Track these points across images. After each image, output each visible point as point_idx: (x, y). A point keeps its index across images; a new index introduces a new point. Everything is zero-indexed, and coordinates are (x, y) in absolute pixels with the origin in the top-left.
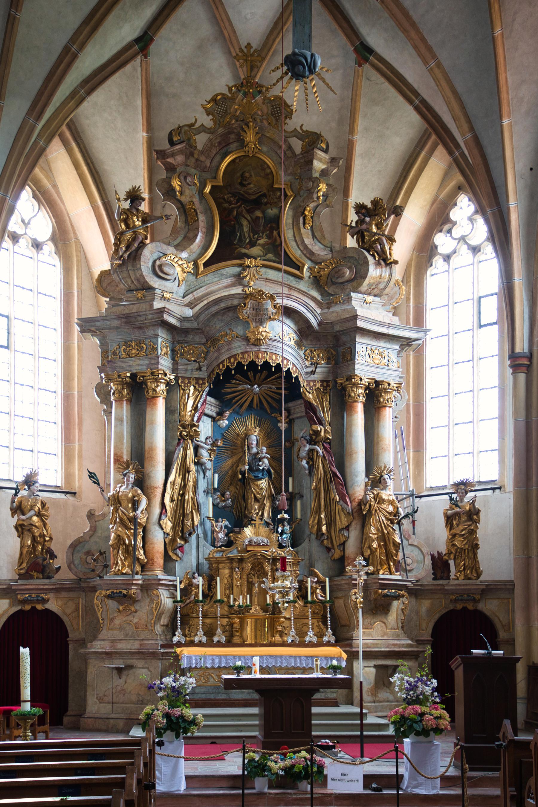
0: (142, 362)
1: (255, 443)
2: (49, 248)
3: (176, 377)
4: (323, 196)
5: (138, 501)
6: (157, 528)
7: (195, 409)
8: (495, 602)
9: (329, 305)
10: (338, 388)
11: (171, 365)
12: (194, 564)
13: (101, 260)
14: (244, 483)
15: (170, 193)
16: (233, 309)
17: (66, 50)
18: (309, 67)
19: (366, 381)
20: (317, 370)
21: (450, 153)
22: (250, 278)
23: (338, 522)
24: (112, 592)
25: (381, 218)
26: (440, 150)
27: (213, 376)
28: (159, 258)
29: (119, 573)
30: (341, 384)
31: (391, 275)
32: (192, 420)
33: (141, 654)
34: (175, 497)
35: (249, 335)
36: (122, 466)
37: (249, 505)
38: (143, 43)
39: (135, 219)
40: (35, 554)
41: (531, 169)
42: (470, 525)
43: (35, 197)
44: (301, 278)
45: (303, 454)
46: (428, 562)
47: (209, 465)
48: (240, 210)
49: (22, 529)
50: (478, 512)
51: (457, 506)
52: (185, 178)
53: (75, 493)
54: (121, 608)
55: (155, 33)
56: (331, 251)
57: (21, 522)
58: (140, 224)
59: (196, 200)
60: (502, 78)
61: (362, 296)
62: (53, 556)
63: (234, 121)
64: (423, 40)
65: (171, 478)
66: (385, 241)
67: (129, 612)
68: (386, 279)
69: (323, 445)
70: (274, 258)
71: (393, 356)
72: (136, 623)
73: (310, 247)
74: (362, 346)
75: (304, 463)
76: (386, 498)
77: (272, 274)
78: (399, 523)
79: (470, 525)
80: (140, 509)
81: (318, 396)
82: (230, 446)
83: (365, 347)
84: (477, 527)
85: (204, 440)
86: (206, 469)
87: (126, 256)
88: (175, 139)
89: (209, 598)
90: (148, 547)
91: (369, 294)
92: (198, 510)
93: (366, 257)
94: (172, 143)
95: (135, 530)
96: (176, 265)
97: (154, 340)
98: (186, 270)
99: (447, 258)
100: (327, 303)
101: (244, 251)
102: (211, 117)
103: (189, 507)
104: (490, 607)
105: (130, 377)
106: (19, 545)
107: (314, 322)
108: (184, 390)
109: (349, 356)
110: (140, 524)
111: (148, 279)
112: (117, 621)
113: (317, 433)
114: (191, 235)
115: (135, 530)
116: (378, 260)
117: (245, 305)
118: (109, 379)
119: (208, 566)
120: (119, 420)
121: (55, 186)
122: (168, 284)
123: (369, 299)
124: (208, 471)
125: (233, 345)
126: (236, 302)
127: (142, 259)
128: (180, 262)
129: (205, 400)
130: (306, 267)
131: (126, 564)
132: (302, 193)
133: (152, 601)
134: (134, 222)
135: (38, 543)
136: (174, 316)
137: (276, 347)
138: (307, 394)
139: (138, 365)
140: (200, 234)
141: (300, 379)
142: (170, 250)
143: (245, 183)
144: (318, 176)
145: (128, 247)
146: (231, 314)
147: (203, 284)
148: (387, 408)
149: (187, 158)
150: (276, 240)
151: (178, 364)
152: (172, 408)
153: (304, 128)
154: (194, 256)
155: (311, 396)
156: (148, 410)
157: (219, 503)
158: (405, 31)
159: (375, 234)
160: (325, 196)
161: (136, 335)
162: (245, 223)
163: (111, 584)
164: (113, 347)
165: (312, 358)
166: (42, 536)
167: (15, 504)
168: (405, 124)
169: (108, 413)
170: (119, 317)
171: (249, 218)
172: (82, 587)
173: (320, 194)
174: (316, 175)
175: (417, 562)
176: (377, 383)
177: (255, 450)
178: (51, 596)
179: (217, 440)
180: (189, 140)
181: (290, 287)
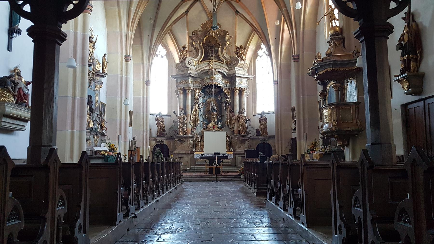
2: (165, 57)
9: (230, 70)
10: (232, 89)
13: (177, 60)
15: (192, 45)
16: (207, 72)
17: (169, 16)
19: (238, 88)
21: (258, 34)
26: (256, 34)
33: (185, 154)
36: (181, 110)
38: (187, 12)
45: (224, 106)
46: (255, 131)
47: (202, 109)
49: (158, 124)
50: (267, 119)
59: (199, 47)
60: (267, 20)
62: (165, 131)
64: (249, 11)
71: (245, 82)
74: (238, 80)
77: (216, 63)
82: (207, 104)
99: (261, 57)
100: (229, 69)
103: (197, 119)
104: (270, 142)
107: (226, 75)
109: (234, 82)
113: (227, 101)
120: (180, 98)
121: (167, 43)
123: (239, 68)
158: (244, 9)
161: (184, 79)
168: (248, 28)
170: (180, 75)
172: (171, 138)
174: (226, 40)
176: (241, 88)
181: (221, 66)
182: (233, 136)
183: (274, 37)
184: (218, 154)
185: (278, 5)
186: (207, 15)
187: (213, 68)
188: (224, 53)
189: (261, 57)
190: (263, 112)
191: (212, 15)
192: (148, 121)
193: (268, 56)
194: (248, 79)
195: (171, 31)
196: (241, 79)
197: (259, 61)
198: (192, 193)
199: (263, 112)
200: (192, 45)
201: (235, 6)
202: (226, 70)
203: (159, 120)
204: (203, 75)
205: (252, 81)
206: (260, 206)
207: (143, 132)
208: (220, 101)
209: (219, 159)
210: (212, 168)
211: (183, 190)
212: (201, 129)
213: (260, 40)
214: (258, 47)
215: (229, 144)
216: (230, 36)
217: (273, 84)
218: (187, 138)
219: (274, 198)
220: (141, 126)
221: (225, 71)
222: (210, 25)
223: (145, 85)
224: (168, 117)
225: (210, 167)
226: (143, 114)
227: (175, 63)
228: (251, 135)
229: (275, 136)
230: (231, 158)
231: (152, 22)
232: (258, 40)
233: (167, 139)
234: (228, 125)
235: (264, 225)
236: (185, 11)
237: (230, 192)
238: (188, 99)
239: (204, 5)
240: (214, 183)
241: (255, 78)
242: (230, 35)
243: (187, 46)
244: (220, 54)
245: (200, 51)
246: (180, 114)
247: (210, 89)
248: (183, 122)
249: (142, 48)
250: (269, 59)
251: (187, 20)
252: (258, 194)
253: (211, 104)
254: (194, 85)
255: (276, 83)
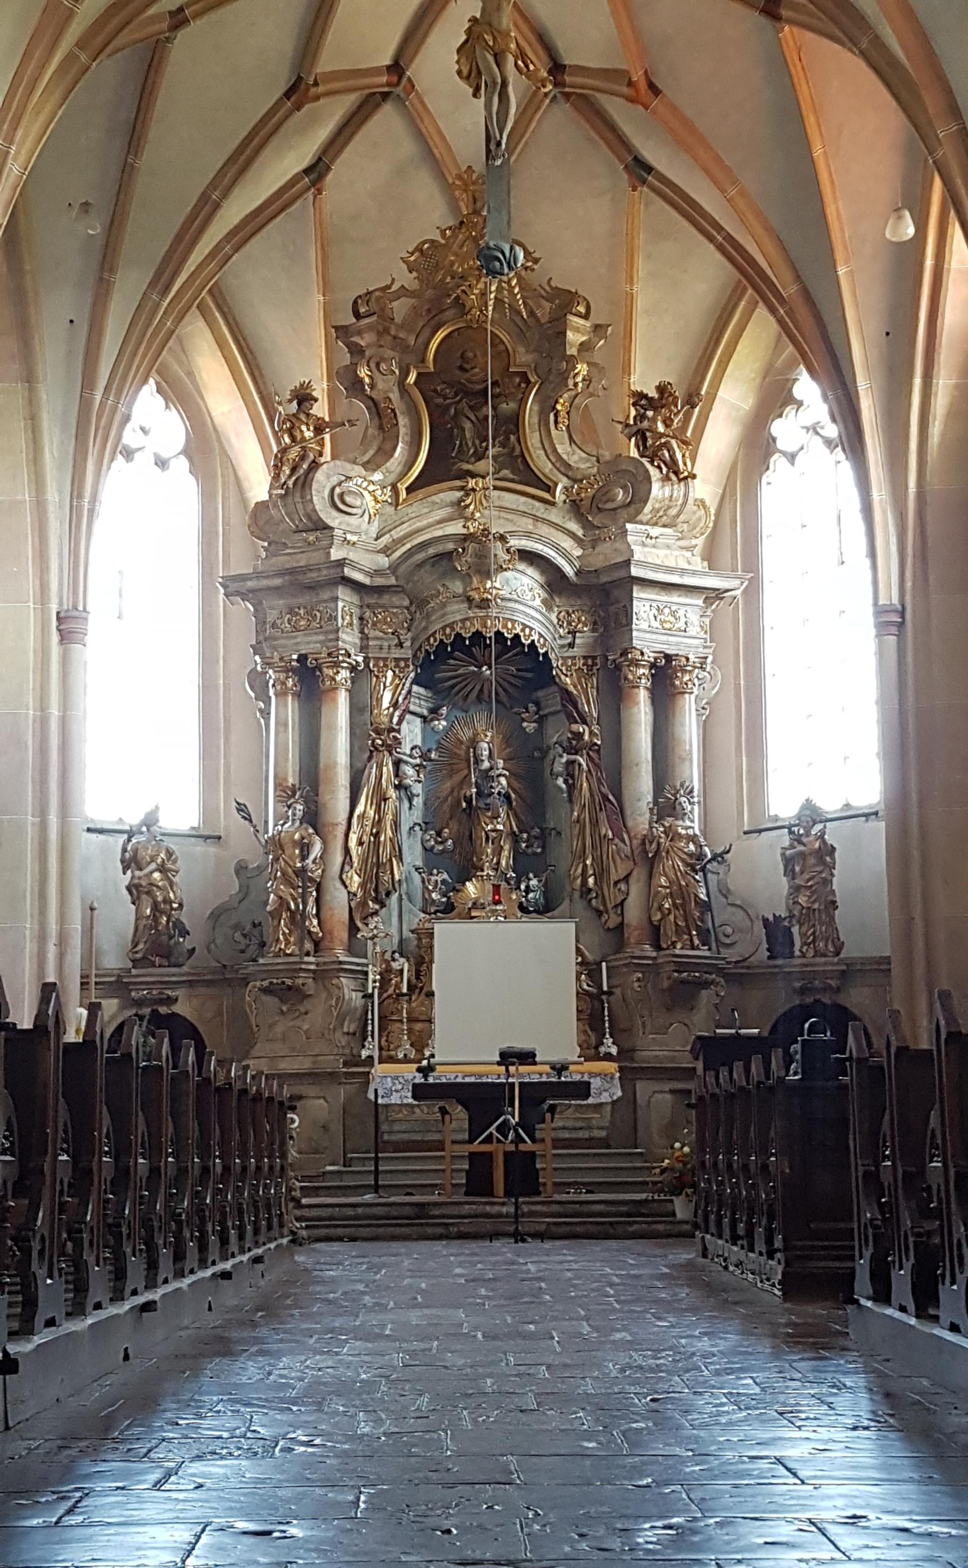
0: (315, 638)
1: (486, 753)
2: (183, 463)
3: (365, 658)
4: (584, 380)
5: (308, 845)
6: (338, 884)
7: (395, 705)
8: (866, 991)
9: (594, 543)
10: (610, 661)
11: (358, 641)
12: (396, 940)
13: (259, 484)
14: (470, 815)
15: (355, 386)
16: (448, 555)
17: (204, 197)
18: (509, 263)
19: (650, 656)
20: (577, 641)
21: (773, 310)
22: (476, 507)
23: (613, 870)
24: (271, 983)
25: (671, 411)
26: (761, 311)
27: (421, 656)
28: (340, 484)
29: (281, 953)
30: (614, 661)
31: (686, 495)
32: (391, 722)
33: (313, 1077)
34: (365, 838)
35: (471, 593)
36: (286, 794)
37: (478, 849)
38: (317, 171)
39: (304, 428)
40: (157, 930)
41: (888, 334)
42: (821, 872)
43: (160, 390)
44: (553, 504)
45: (558, 768)
46: (760, 931)
47: (418, 789)
48: (460, 406)
51: (800, 842)
52: (378, 365)
53: (219, 838)
54: (284, 1008)
55: (333, 161)
56: (598, 461)
57: (136, 881)
58: (312, 435)
59: (395, 396)
60: (831, 211)
61: (643, 527)
62: (185, 933)
63: (448, 280)
64: (718, 160)
65: (360, 809)
66: (675, 446)
67: (297, 1014)
68: (680, 502)
69: (588, 754)
70: (511, 476)
71: (694, 617)
72: (308, 1030)
73: (565, 457)
75: (560, 782)
76: (683, 832)
77: (509, 499)
78: (703, 869)
79: (821, 872)
80: (312, 857)
81: (579, 679)
82: (448, 759)
83: (647, 604)
84: (832, 875)
85: (408, 752)
86: (413, 795)
87: (290, 483)
88: (362, 310)
89: (417, 991)
90: (325, 914)
91: (656, 524)
92: (400, 858)
93: (647, 471)
94: (357, 315)
95: (304, 888)
96: (365, 493)
97: (332, 605)
98: (379, 498)
99: (791, 458)
100: (589, 542)
101: (466, 467)
102: (415, 274)
103: (385, 853)
105: (298, 661)
106: (132, 918)
107: (569, 570)
108: (377, 677)
110: (311, 880)
111: (322, 515)
112: (279, 1029)
113: (580, 736)
114: (388, 446)
115: (304, 888)
116: (667, 475)
117: (464, 549)
118: (267, 664)
119: (415, 942)
120: (282, 724)
121: (190, 374)
122: (353, 520)
123: (655, 531)
124: (416, 799)
125: (449, 609)
126: (451, 546)
127: (315, 486)
128: (371, 488)
129: (409, 692)
130: (560, 487)
131: (292, 939)
132: (551, 378)
133: (330, 996)
134: (302, 431)
135: (162, 912)
136: (360, 570)
137: (514, 610)
138: (563, 677)
139: (309, 643)
140: (400, 444)
141: (552, 656)
142: (358, 469)
143: (466, 366)
144: (575, 353)
145: (294, 470)
146: (444, 563)
147: (406, 519)
148: (687, 696)
149: (380, 334)
150: (513, 449)
151: (368, 639)
152: (361, 705)
153: (553, 284)
154: (392, 478)
155: (568, 680)
156: (324, 710)
157: (433, 847)
159: (662, 435)
160: (587, 380)
162: (468, 426)
163: (269, 972)
164: (272, 615)
165: (569, 624)
166: (167, 901)
167: (127, 855)
168: (706, 273)
169: (266, 714)
170: (280, 573)
171: (473, 418)
172: (225, 979)
173: (579, 379)
174: (572, 351)
175: (741, 931)
176: (668, 658)
177: (486, 765)
178: (179, 993)
179: (429, 751)
180: (383, 309)
181: (536, 519)
182: (620, 960)
183: (875, 327)
184: (527, 1057)
185: (905, 109)
186: (448, 189)
187: (486, 532)
188: (559, 436)
189: (791, 458)
190: (808, 805)
191: (479, 194)
192: (75, 866)
193: (839, 454)
194: (713, 596)
195: (218, 295)
196: (664, 597)
197: (778, 487)
198: (361, 1287)
199: (808, 805)
200: (355, 386)
201: (627, 129)
202: (567, 543)
203: (142, 856)
204: (427, 577)
205: (737, 612)
206: (816, 1342)
207: (42, 938)
208: (534, 738)
209: (535, 1095)
210: (489, 1156)
211: (305, 1276)
212: (415, 918)
213: (791, 348)
214: (775, 398)
215: (594, 1013)
216: (597, 327)
217: (872, 631)
218: (322, 975)
219: (902, 1278)
220: (29, 904)
221: (566, 553)
222: (472, 245)
223: (55, 637)
224: (199, 848)
225: (476, 1147)
226: (43, 826)
227: (243, 500)
228: (731, 955)
229: (887, 960)
230: (605, 1098)
231: (95, 229)
232: (777, 348)
233: (191, 984)
234: (585, 891)
235: (850, 1421)
236: (305, 164)
237: (611, 1285)
238: (333, 727)
239: (427, 127)
240: (505, 1249)
241: (754, 590)
242: (595, 318)
243: (320, 390)
244: (533, 439)
245: (403, 421)
246: (276, 820)
247: (467, 665)
248: (301, 873)
249: (32, 403)
250: (846, 470)
251: (320, 224)
252: (794, 1287)
253: (478, 761)
254: (365, 637)
255: (892, 621)
